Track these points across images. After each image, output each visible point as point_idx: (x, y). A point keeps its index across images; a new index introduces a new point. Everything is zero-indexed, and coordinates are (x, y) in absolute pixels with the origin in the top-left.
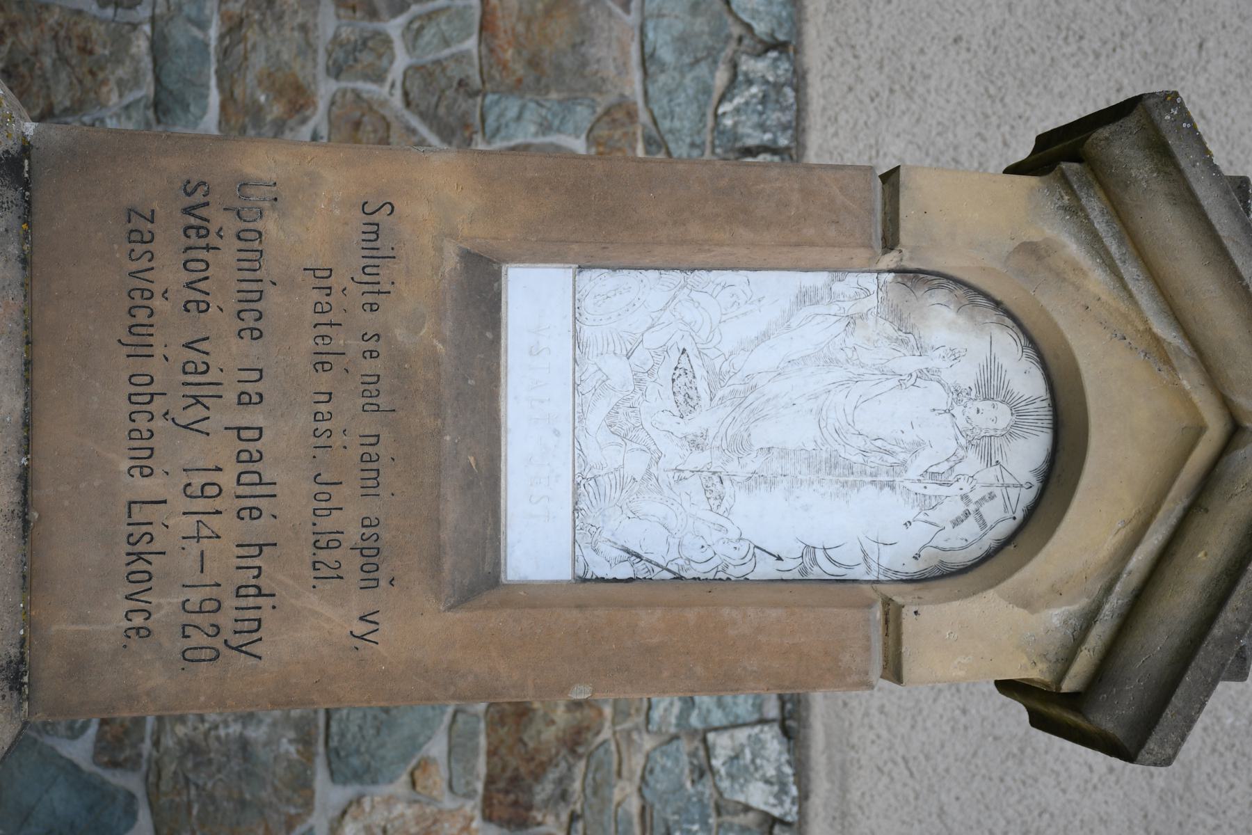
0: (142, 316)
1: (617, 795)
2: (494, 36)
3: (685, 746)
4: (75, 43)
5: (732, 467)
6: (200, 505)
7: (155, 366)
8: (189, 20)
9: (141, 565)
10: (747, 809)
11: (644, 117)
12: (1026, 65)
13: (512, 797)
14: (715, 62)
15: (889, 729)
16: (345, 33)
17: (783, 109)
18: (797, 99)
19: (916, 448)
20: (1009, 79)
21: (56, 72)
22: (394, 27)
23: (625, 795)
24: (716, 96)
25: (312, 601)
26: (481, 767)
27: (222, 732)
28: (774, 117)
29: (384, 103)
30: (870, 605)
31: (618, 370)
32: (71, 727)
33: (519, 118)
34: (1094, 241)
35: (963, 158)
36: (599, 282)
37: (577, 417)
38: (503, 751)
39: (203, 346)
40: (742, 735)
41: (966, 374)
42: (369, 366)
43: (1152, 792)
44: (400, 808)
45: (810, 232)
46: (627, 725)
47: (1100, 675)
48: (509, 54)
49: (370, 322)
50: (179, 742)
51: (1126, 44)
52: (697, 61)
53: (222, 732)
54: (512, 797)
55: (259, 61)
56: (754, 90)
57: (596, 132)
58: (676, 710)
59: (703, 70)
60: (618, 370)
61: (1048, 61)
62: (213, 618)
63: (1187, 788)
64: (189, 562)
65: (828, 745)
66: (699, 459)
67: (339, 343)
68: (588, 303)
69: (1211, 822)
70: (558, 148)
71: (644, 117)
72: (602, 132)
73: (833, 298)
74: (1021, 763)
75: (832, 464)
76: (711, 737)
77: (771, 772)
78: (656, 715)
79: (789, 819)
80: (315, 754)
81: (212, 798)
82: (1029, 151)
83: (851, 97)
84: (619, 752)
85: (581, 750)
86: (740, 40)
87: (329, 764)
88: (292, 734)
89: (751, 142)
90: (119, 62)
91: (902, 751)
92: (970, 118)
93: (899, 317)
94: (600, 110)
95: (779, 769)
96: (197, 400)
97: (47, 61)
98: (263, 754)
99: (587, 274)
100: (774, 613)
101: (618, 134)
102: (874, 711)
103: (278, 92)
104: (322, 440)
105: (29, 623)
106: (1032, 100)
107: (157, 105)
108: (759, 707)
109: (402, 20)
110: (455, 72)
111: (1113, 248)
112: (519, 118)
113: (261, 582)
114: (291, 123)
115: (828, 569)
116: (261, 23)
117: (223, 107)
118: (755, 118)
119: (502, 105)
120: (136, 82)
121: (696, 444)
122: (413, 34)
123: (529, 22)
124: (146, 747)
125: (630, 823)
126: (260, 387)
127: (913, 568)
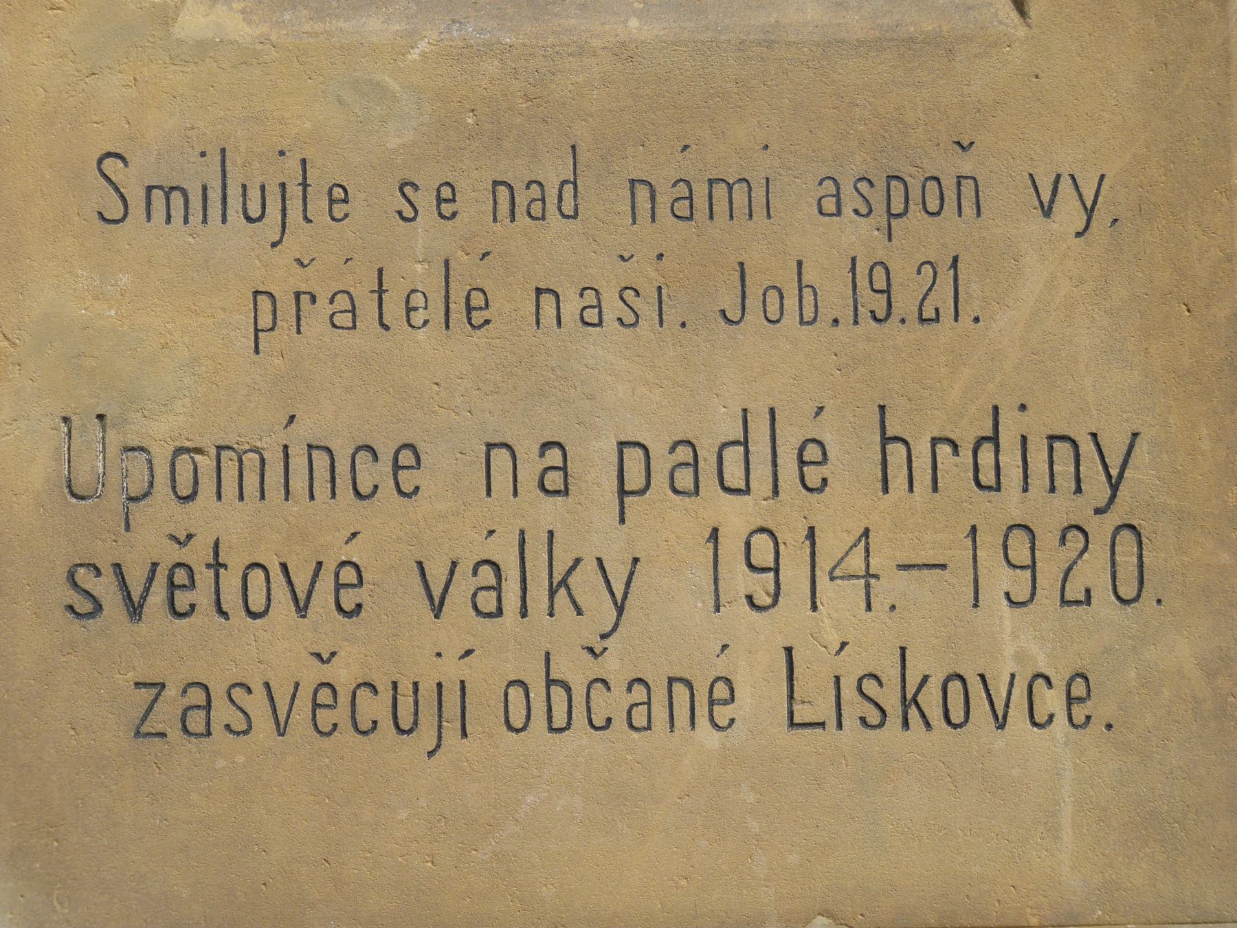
0: (373, 707)
6: (794, 573)
67: (425, 276)
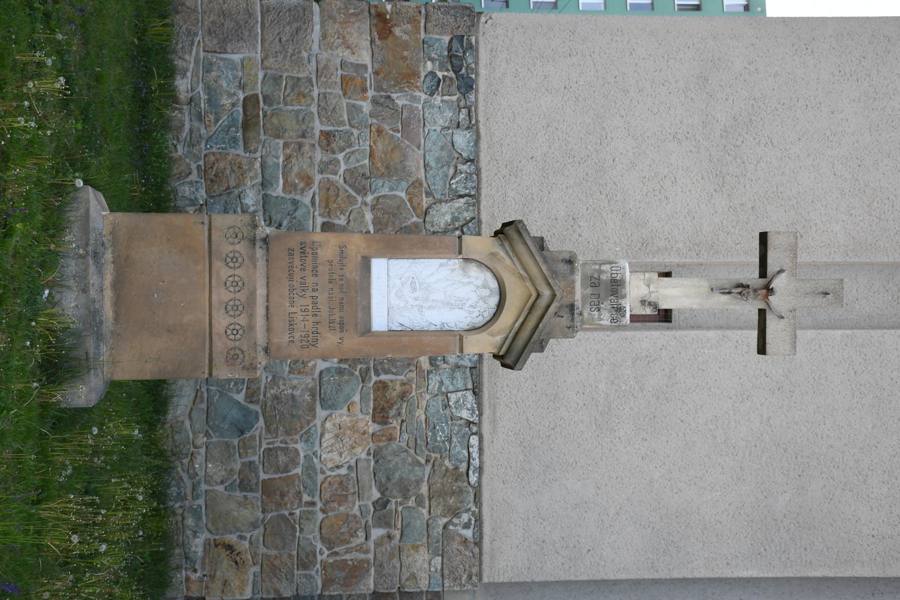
0: (291, 272)
1: (417, 414)
2: (374, 159)
3: (440, 398)
4: (237, 165)
5: (425, 305)
6: (304, 313)
7: (294, 283)
8: (273, 156)
10: (461, 419)
11: (425, 185)
12: (556, 166)
14: (449, 166)
15: (510, 392)
16: (324, 159)
17: (473, 182)
18: (477, 178)
20: (550, 171)
21: (231, 175)
22: (341, 156)
23: (420, 414)
24: (450, 178)
25: (329, 335)
26: (372, 405)
27: (286, 392)
28: (470, 184)
29: (337, 182)
30: (456, 336)
31: (398, 282)
32: (237, 390)
33: (383, 186)
34: (507, 252)
35: (535, 198)
36: (393, 262)
37: (389, 293)
38: (379, 399)
40: (459, 394)
41: (479, 283)
42: (341, 282)
43: (598, 411)
44: (345, 418)
45: (441, 251)
46: (421, 391)
47: (508, 351)
48: (379, 165)
49: (341, 272)
50: (272, 395)
52: (443, 166)
53: (286, 392)
55: (296, 169)
56: (463, 175)
58: (437, 386)
59: (445, 168)
60: (398, 282)
63: (609, 410)
64: (302, 326)
65: (489, 398)
66: (417, 303)
67: (334, 277)
68: (391, 267)
69: (617, 421)
70: (396, 196)
72: (411, 190)
73: (448, 265)
75: (448, 304)
76: (449, 395)
77: (469, 406)
78: (430, 387)
80: (316, 400)
81: (283, 413)
83: (496, 177)
85: (405, 399)
86: (458, 158)
88: (309, 393)
89: (461, 193)
90: (251, 171)
91: (514, 399)
92: (537, 184)
93: (463, 269)
94: (410, 183)
95: (472, 405)
96: (303, 290)
97: (228, 172)
98: (299, 400)
100: (433, 338)
101: (416, 191)
102: (505, 386)
104: (330, 299)
105: (269, 339)
106: (558, 178)
107: (262, 184)
108: (465, 385)
109: (343, 154)
110: (361, 171)
111: (511, 254)
112: (383, 186)
113: (318, 331)
114: (306, 189)
115: (447, 328)
116: (296, 156)
117: (284, 184)
118: (463, 185)
120: (256, 177)
121: (416, 299)
122: (347, 159)
123: (386, 154)
124: (261, 397)
125: (422, 423)
127: (467, 328)
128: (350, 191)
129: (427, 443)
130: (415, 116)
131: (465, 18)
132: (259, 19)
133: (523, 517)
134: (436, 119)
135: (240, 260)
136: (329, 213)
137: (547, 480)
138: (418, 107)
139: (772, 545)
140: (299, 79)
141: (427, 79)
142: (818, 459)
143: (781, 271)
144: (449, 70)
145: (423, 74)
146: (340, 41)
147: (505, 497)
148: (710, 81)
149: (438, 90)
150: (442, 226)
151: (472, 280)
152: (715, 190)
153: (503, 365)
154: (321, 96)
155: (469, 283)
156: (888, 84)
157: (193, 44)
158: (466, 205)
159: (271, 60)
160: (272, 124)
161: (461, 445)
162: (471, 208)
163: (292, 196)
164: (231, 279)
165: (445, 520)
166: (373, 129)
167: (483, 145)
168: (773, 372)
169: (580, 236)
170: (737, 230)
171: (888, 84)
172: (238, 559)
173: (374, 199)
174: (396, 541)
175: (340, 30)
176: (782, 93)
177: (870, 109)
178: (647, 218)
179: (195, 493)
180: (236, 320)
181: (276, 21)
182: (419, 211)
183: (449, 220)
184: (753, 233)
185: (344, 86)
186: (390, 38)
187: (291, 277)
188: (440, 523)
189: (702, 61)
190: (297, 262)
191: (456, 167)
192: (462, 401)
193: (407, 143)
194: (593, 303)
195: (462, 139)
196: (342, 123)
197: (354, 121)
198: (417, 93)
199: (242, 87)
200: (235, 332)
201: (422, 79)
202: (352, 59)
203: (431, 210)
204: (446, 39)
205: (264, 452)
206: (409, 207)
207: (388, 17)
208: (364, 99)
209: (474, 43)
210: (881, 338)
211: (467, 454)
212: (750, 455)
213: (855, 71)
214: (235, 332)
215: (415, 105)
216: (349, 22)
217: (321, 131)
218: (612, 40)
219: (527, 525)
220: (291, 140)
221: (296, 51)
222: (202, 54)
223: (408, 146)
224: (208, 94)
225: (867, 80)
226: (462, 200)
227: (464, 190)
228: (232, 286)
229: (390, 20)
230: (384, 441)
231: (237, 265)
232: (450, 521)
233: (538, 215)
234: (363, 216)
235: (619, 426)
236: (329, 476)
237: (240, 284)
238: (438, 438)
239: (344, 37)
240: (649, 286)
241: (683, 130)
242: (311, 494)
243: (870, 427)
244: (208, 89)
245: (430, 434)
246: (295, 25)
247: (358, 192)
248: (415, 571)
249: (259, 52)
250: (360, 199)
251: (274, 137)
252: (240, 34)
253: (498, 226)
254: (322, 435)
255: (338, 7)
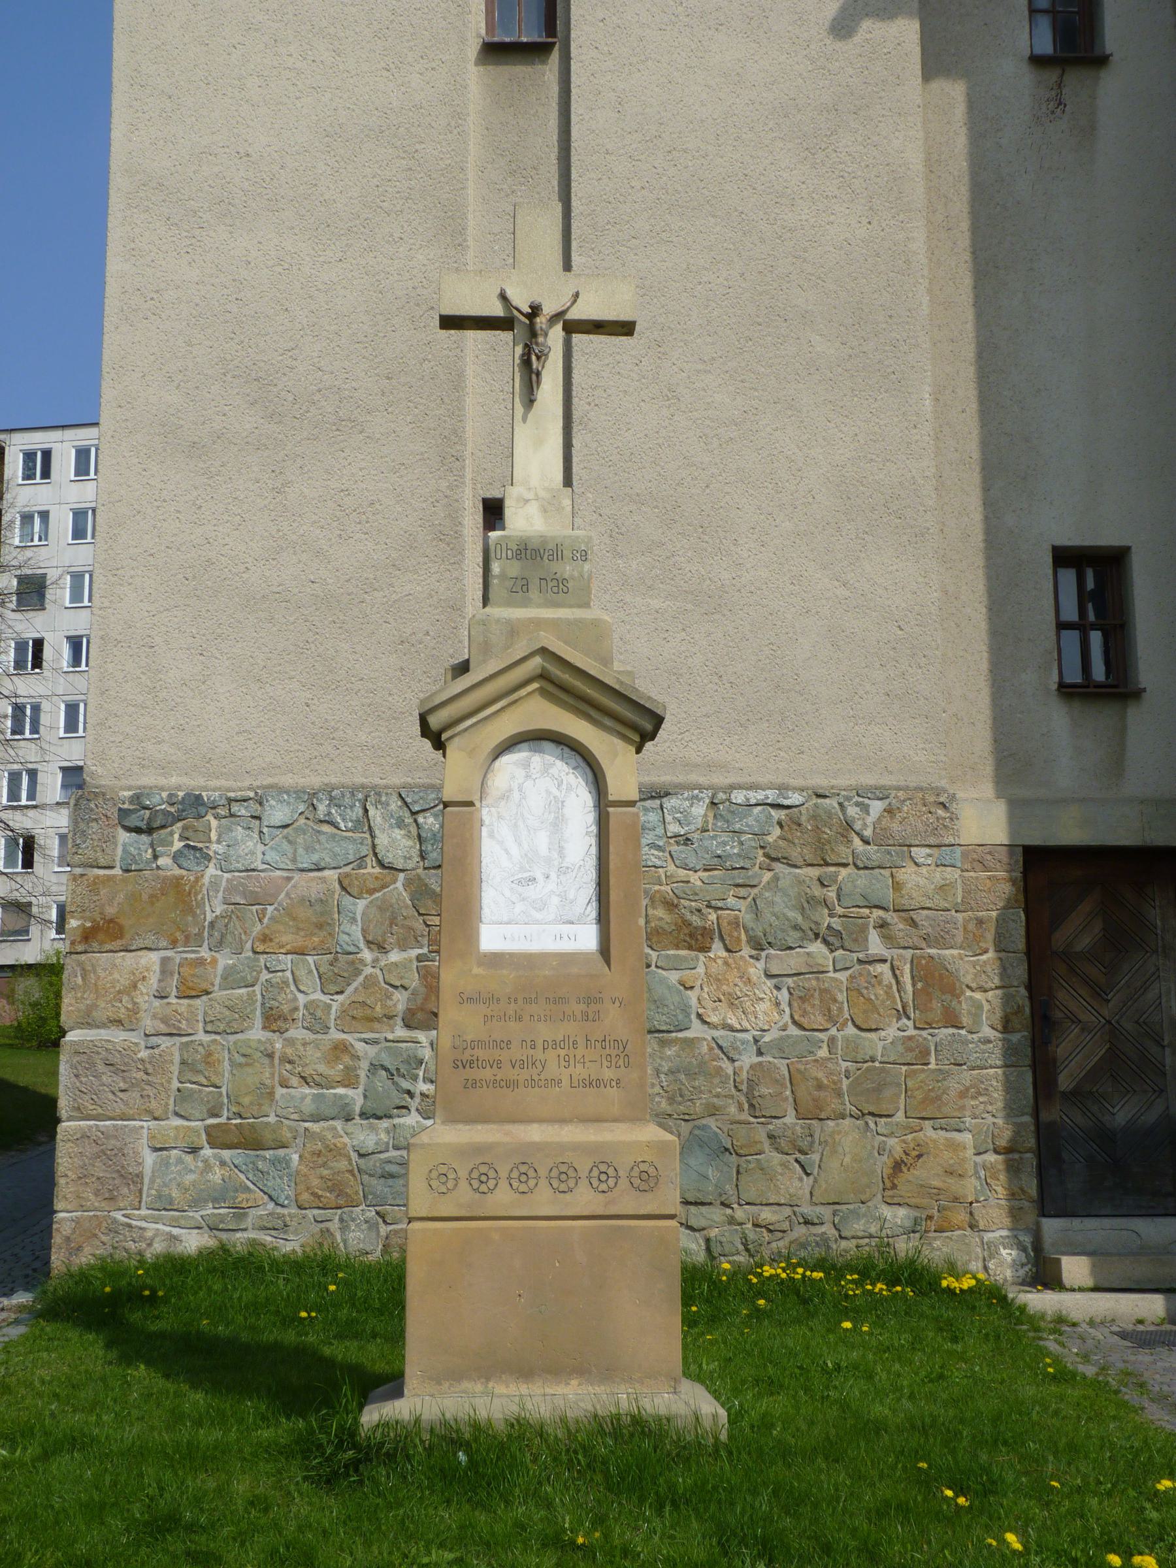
0: (503, 1084)
2: (307, 947)
5: (556, 863)
6: (572, 1062)
8: (302, 1102)
9: (594, 1083)
10: (705, 815)
13: (699, 937)
15: (665, 742)
19: (548, 792)
28: (347, 800)
31: (519, 907)
36: (487, 913)
37: (537, 922)
39: (514, 1062)
40: (668, 818)
41: (520, 773)
42: (520, 1001)
47: (634, 727)
51: (311, 619)
52: (319, 841)
54: (699, 937)
55: (322, 1068)
56: (333, 811)
57: (355, 895)
59: (323, 838)
60: (519, 907)
61: (318, 659)
62: (613, 1057)
66: (553, 876)
71: (348, 869)
74: (681, 675)
76: (669, 834)
79: (710, 795)
80: (676, 1037)
82: (427, 740)
83: (336, 760)
84: (677, 882)
87: (681, 1030)
88: (667, 1049)
95: (687, 799)
97: (325, 1172)
99: (483, 919)
101: (356, 883)
103: (337, 1059)
117: (346, 1086)
119: (343, 943)
126: (529, 1042)
128: (355, 985)
129: (742, 868)
130: (242, 884)
131: (93, 806)
132: (92, 1123)
133: (851, 724)
134: (246, 851)
135: (483, 1169)
136: (390, 1018)
137: (797, 688)
138: (228, 880)
139: (886, 363)
140: (183, 1063)
141: (185, 865)
142: (761, 294)
143: (503, 297)
144: (172, 830)
145: (178, 872)
146: (125, 999)
147: (823, 751)
148: (196, 440)
149: (201, 849)
150: (410, 843)
151: (515, 786)
152: (361, 432)
153: (652, 736)
154: (209, 1028)
155: (520, 790)
156: (209, 185)
157: (130, 1226)
158: (379, 807)
159: (154, 1104)
160: (251, 1103)
161: (745, 817)
162: (383, 799)
163: (362, 1074)
164: (515, 1184)
165: (857, 842)
166: (260, 949)
167: (287, 780)
168: (633, 353)
169: (427, 633)
170: (421, 401)
171: (209, 185)
172: (915, 1153)
173: (369, 948)
174: (890, 917)
175: (109, 999)
176: (217, 334)
177: (244, 210)
178: (402, 533)
179: (816, 1221)
180: (583, 1174)
181: (94, 1097)
182: (388, 879)
183: (402, 832)
184: (426, 378)
185: (194, 993)
186: (122, 921)
187: (512, 1084)
188: (861, 848)
189: (165, 450)
190: (487, 1074)
191: (321, 821)
192: (679, 815)
193: (282, 895)
194: (555, 589)
195: (277, 813)
196: (251, 996)
197: (249, 977)
198: (206, 880)
199: (194, 1150)
200: (603, 1177)
201: (184, 872)
202: (153, 981)
203: (386, 861)
204: (123, 836)
205: (756, 1117)
206: (380, 894)
207: (89, 925)
208: (214, 961)
209: (131, 793)
210: (583, 201)
211: (759, 808)
212: (756, 390)
213: (188, 231)
214: (603, 1177)
215: (224, 883)
216: (95, 985)
217: (264, 1028)
218: (130, 584)
219: (863, 718)
220: (277, 1075)
221: (140, 1067)
222: (144, 1212)
223: (288, 894)
224: (206, 1201)
225: (200, 214)
226: (371, 812)
227: (356, 809)
228: (526, 1182)
229: (93, 921)
230: (740, 934)
231: (492, 1174)
232: (858, 834)
233: (395, 697)
234: (396, 964)
235: (716, 580)
236: (792, 1017)
237: (523, 1169)
238: (736, 851)
239: (119, 992)
240: (527, 501)
241: (269, 478)
242: (818, 1044)
243: (712, 220)
244: (196, 1203)
245: (728, 863)
246: (101, 1067)
247: (358, 972)
248: (933, 887)
249: (141, 1123)
250: (368, 970)
251: (272, 1100)
252: (113, 1153)
253: (427, 744)
254: (732, 1029)
255: (73, 1002)
